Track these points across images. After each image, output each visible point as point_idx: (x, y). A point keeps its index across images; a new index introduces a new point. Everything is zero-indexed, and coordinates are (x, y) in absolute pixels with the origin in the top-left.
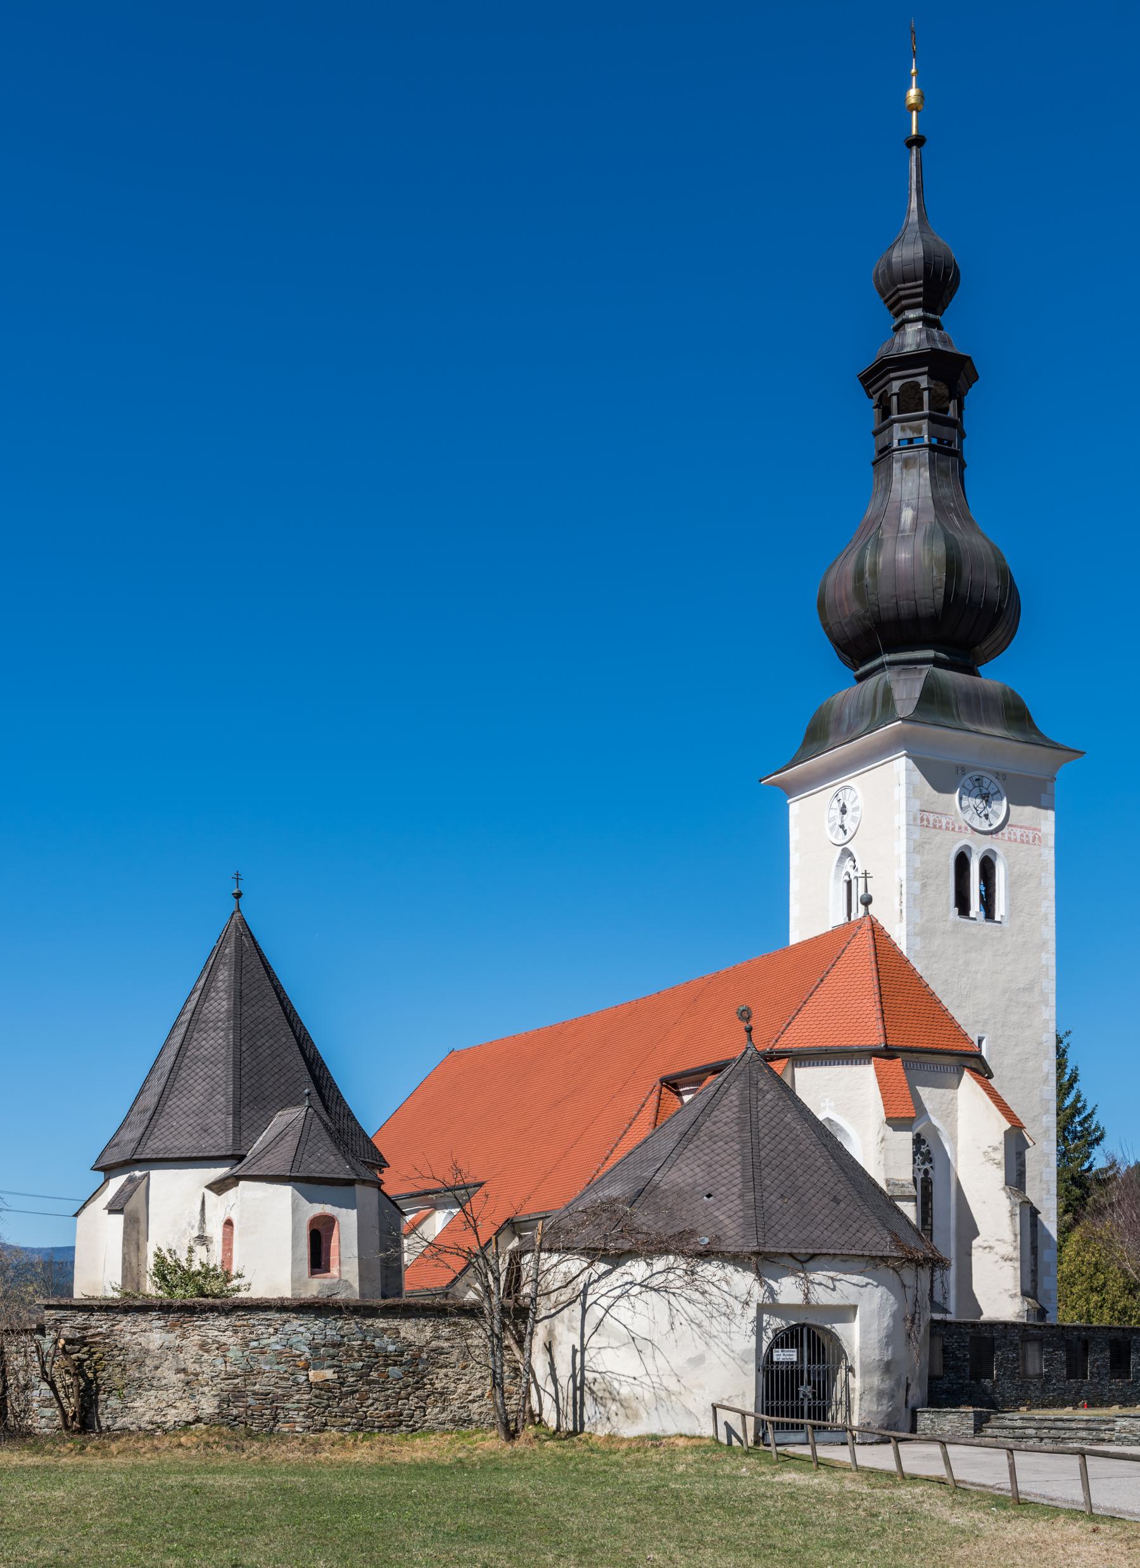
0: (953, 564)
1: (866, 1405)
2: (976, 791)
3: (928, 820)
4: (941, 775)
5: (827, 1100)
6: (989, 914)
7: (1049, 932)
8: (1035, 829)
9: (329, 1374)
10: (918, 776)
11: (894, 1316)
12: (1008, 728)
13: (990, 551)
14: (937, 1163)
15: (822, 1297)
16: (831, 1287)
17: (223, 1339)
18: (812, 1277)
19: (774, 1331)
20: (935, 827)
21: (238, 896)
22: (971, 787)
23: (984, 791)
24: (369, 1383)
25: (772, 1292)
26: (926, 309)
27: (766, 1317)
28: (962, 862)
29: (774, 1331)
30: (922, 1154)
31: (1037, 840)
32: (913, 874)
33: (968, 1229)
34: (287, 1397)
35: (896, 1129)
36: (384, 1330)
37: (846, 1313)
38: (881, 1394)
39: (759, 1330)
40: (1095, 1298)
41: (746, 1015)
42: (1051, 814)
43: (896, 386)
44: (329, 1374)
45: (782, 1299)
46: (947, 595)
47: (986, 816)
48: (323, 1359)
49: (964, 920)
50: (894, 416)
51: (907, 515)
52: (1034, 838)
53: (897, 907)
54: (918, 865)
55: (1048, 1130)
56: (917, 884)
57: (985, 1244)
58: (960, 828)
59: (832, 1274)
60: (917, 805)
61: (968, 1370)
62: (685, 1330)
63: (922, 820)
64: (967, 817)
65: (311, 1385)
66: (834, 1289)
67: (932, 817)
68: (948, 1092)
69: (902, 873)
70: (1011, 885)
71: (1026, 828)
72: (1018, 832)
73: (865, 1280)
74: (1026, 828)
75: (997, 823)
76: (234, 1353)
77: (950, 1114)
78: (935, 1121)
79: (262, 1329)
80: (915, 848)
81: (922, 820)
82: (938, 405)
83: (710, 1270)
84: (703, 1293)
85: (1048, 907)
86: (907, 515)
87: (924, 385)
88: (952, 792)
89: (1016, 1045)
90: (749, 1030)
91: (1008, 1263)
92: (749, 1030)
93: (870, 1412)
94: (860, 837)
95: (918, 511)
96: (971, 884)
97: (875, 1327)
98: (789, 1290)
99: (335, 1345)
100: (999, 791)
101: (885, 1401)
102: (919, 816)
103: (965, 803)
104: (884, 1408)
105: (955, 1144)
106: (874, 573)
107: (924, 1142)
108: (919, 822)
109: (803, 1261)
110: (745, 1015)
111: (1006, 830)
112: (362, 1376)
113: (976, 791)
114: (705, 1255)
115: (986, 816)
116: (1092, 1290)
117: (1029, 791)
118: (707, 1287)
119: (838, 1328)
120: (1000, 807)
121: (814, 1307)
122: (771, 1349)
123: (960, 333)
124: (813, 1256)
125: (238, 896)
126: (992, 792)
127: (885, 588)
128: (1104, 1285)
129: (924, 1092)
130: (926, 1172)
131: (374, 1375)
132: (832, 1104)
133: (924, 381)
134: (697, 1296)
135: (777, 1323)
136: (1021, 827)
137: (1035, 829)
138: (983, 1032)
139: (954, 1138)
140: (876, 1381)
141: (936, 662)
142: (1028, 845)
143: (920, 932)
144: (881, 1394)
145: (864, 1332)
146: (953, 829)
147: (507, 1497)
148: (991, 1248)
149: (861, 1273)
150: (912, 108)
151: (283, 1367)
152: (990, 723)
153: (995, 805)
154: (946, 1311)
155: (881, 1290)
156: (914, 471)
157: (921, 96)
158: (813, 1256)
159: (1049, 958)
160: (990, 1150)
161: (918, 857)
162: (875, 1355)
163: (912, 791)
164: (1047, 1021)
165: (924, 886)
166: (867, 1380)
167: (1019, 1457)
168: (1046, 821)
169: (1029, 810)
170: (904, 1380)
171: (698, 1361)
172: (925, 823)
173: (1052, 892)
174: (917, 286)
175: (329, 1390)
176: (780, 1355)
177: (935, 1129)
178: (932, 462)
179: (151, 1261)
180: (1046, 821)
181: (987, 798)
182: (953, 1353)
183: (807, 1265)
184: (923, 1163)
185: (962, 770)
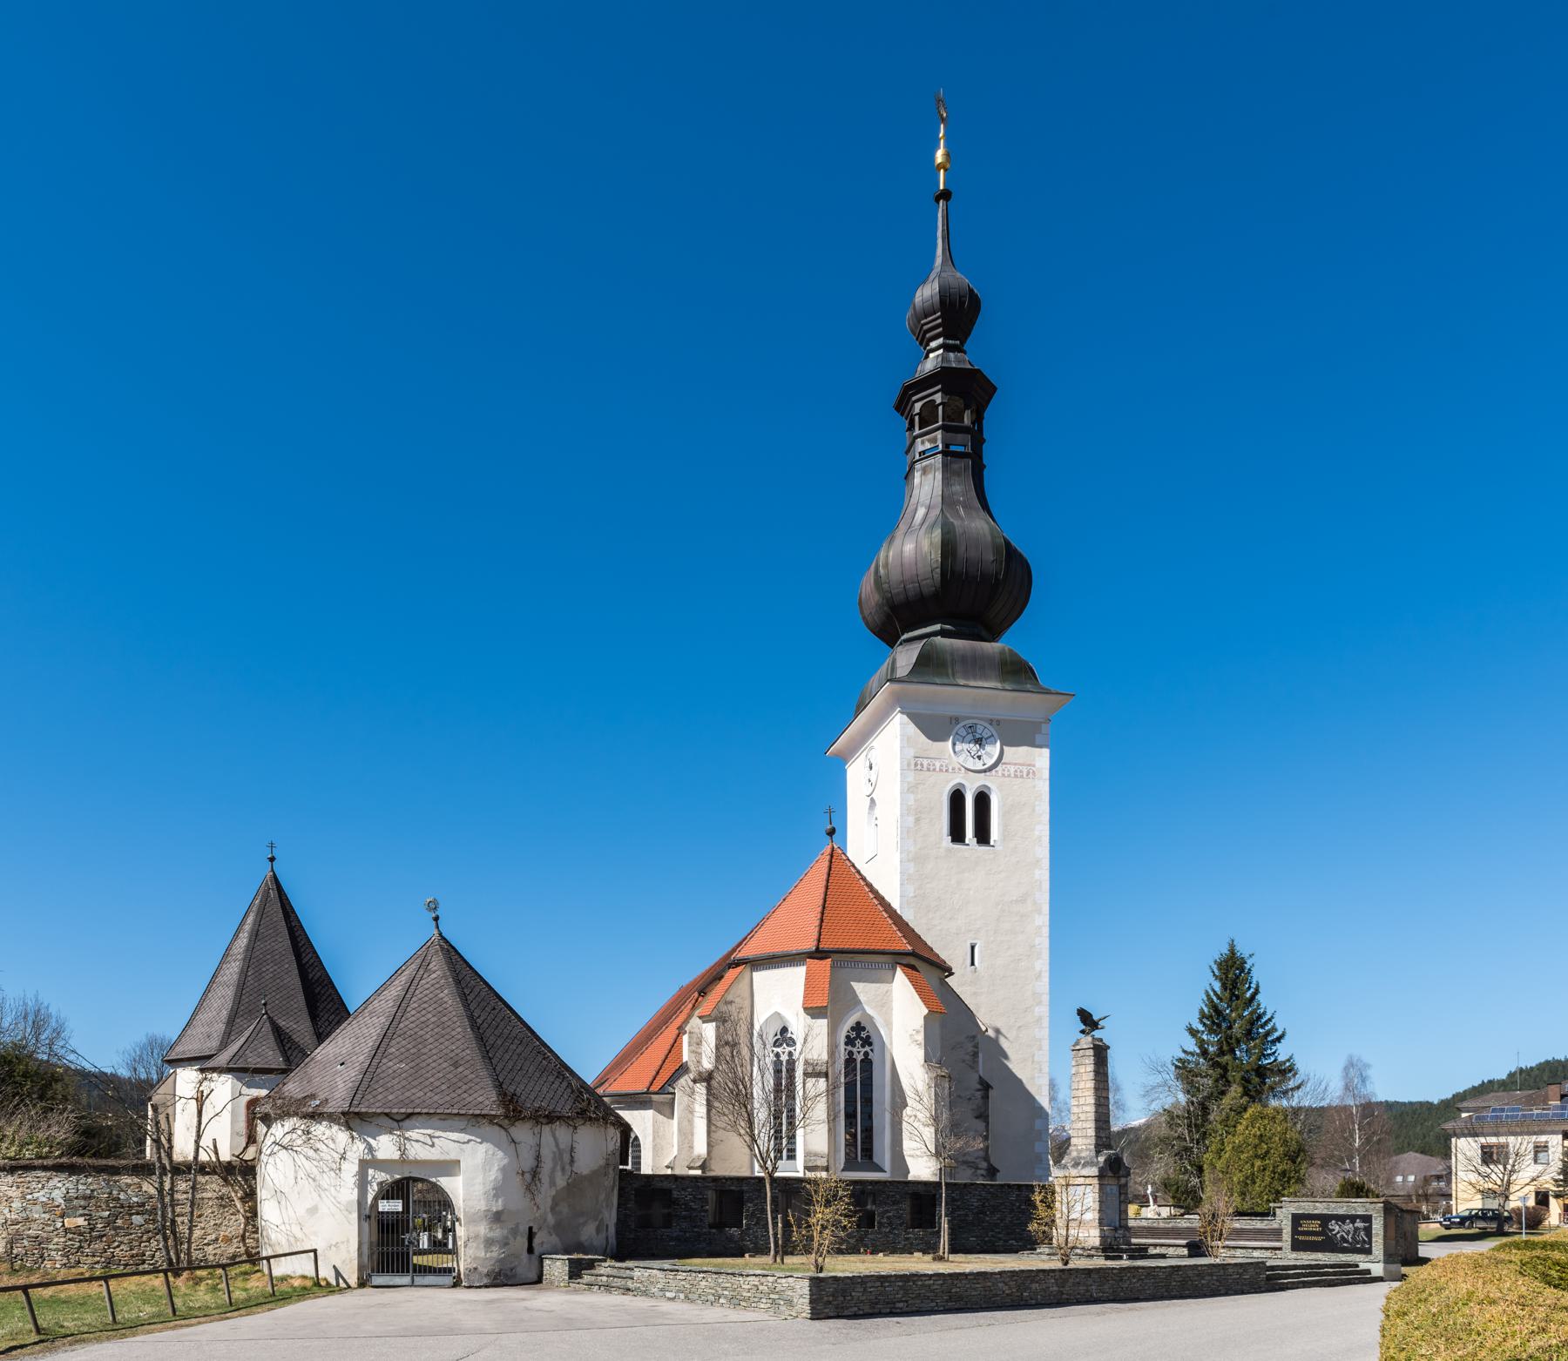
0: (948, 547)
1: (471, 1252)
2: (970, 737)
4: (934, 727)
6: (983, 836)
7: (1043, 851)
9: (81, 1221)
10: (912, 729)
11: (503, 1170)
12: (1003, 681)
14: (876, 1047)
15: (418, 1152)
16: (426, 1145)
17: (10, 1194)
18: (408, 1134)
19: (380, 1184)
21: (272, 859)
24: (115, 1229)
25: (370, 1149)
26: (946, 338)
27: (371, 1172)
28: (957, 798)
29: (380, 1184)
31: (1031, 774)
32: (906, 810)
33: (899, 1101)
34: (49, 1240)
35: (814, 1016)
36: (129, 1186)
37: (450, 1167)
38: (489, 1243)
39: (363, 1183)
40: (1258, 1163)
42: (1046, 752)
43: (918, 406)
44: (81, 1221)
45: (380, 1155)
46: (943, 574)
48: (75, 1208)
49: (984, 848)
50: (917, 432)
51: (921, 512)
54: (911, 802)
56: (911, 819)
59: (429, 1131)
60: (911, 752)
62: (305, 1184)
63: (916, 765)
64: (961, 759)
65: (67, 1231)
66: (433, 1146)
67: (925, 762)
68: (883, 987)
70: (1004, 815)
72: (1012, 769)
73: (468, 1137)
75: (990, 762)
76: (16, 1205)
77: (885, 1004)
78: (869, 1011)
79: (34, 1185)
80: (909, 789)
82: (952, 416)
83: (321, 1129)
84: (316, 1150)
85: (1042, 830)
86: (921, 512)
87: (939, 401)
88: (943, 739)
90: (436, 919)
92: (436, 919)
93: (475, 1258)
94: (887, 784)
95: (929, 508)
96: (969, 818)
97: (480, 1179)
98: (386, 1146)
99: (85, 1198)
101: (495, 1248)
103: (958, 747)
104: (495, 1254)
105: (891, 1030)
106: (886, 565)
107: (864, 1029)
109: (398, 1120)
110: (433, 906)
111: (999, 768)
112: (109, 1223)
113: (970, 737)
114: (315, 1116)
116: (1257, 1156)
117: (1018, 734)
118: (319, 1145)
119: (444, 1182)
120: (993, 750)
121: (411, 1162)
122: (375, 1199)
123: (978, 354)
124: (409, 1116)
125: (272, 859)
127: (895, 576)
128: (1267, 1152)
129: (860, 988)
131: (119, 1222)
133: (938, 398)
134: (311, 1153)
135: (382, 1176)
139: (889, 1024)
140: (483, 1229)
141: (943, 633)
142: (1022, 782)
143: (914, 861)
144: (489, 1243)
145: (467, 1185)
149: (462, 1131)
150: (940, 166)
151: (47, 1216)
152: (984, 677)
153: (988, 748)
154: (882, 1170)
155: (485, 1146)
156: (931, 476)
157: (947, 155)
158: (409, 1116)
159: (1043, 874)
161: (912, 797)
162: (481, 1205)
163: (906, 741)
164: (1040, 927)
165: (917, 820)
166: (472, 1229)
168: (1041, 758)
169: (1024, 750)
170: (524, 1229)
171: (313, 1211)
173: (1046, 817)
174: (936, 319)
175: (81, 1234)
176: (384, 1206)
177: (871, 1018)
178: (945, 466)
180: (1041, 758)
181: (979, 741)
183: (407, 1123)
185: (957, 720)
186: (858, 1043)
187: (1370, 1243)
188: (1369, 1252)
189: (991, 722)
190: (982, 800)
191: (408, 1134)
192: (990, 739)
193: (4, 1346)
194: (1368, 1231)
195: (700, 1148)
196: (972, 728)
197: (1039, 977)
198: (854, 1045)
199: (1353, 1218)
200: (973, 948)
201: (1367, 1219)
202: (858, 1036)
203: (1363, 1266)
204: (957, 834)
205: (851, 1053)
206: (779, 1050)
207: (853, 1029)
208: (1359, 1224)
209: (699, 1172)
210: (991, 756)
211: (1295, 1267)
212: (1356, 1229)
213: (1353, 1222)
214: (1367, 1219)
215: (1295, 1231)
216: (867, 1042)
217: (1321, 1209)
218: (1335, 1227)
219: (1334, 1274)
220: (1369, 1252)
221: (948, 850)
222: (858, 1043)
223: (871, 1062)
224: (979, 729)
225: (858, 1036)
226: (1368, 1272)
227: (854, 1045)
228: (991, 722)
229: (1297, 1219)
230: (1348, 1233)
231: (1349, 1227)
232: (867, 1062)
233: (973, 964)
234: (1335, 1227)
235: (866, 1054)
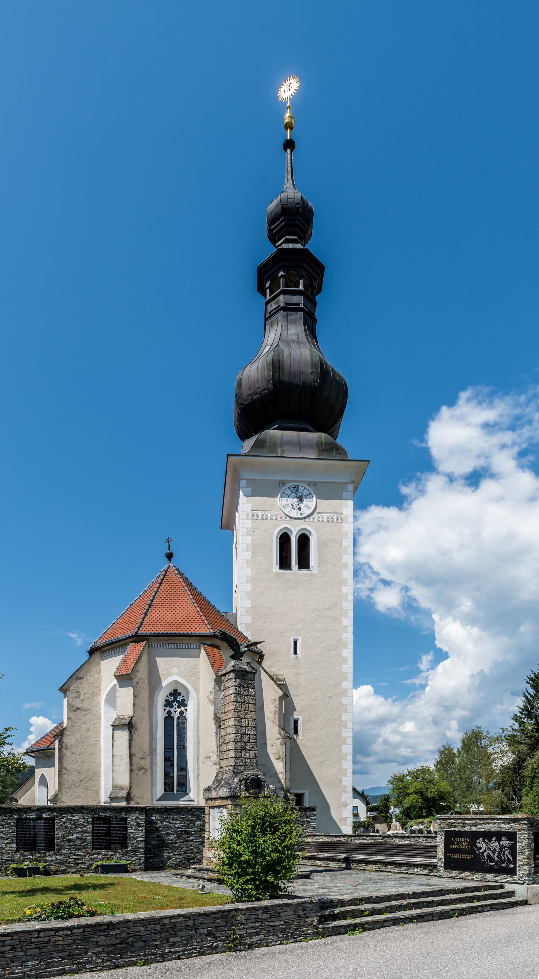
2: (294, 495)
3: (257, 516)
6: (304, 563)
8: (338, 513)
13: (289, 365)
20: (262, 519)
22: (289, 493)
23: (299, 494)
28: (284, 539)
31: (340, 519)
47: (300, 509)
49: (304, 572)
52: (337, 519)
58: (281, 518)
67: (260, 514)
71: (331, 513)
74: (331, 513)
75: (307, 512)
81: (253, 516)
88: (276, 496)
89: (322, 642)
100: (310, 493)
102: (251, 514)
108: (250, 517)
111: (315, 515)
115: (300, 509)
120: (309, 504)
136: (328, 513)
137: (338, 513)
138: (297, 635)
147: (223, 880)
148: (210, 757)
172: (255, 517)
179: (348, 734)
184: (179, 707)
185: (283, 483)
186: (175, 704)
187: (515, 863)
188: (512, 872)
189: (309, 484)
190: (304, 540)
192: (309, 495)
193: (4, 890)
194: (513, 849)
196: (295, 489)
197: (345, 660)
198: (172, 707)
199: (499, 835)
200: (296, 643)
201: (512, 836)
203: (508, 887)
204: (284, 563)
205: (169, 713)
208: (505, 842)
209: (124, 804)
210: (309, 508)
211: (369, 900)
212: (502, 848)
213: (499, 840)
214: (512, 836)
215: (447, 850)
217: (469, 826)
218: (482, 844)
219: (461, 900)
220: (512, 872)
221: (278, 574)
222: (175, 704)
224: (301, 489)
225: (175, 700)
226: (511, 894)
227: (172, 707)
228: (309, 484)
229: (450, 836)
230: (494, 851)
231: (495, 845)
233: (295, 653)
234: (482, 844)
235: (182, 713)
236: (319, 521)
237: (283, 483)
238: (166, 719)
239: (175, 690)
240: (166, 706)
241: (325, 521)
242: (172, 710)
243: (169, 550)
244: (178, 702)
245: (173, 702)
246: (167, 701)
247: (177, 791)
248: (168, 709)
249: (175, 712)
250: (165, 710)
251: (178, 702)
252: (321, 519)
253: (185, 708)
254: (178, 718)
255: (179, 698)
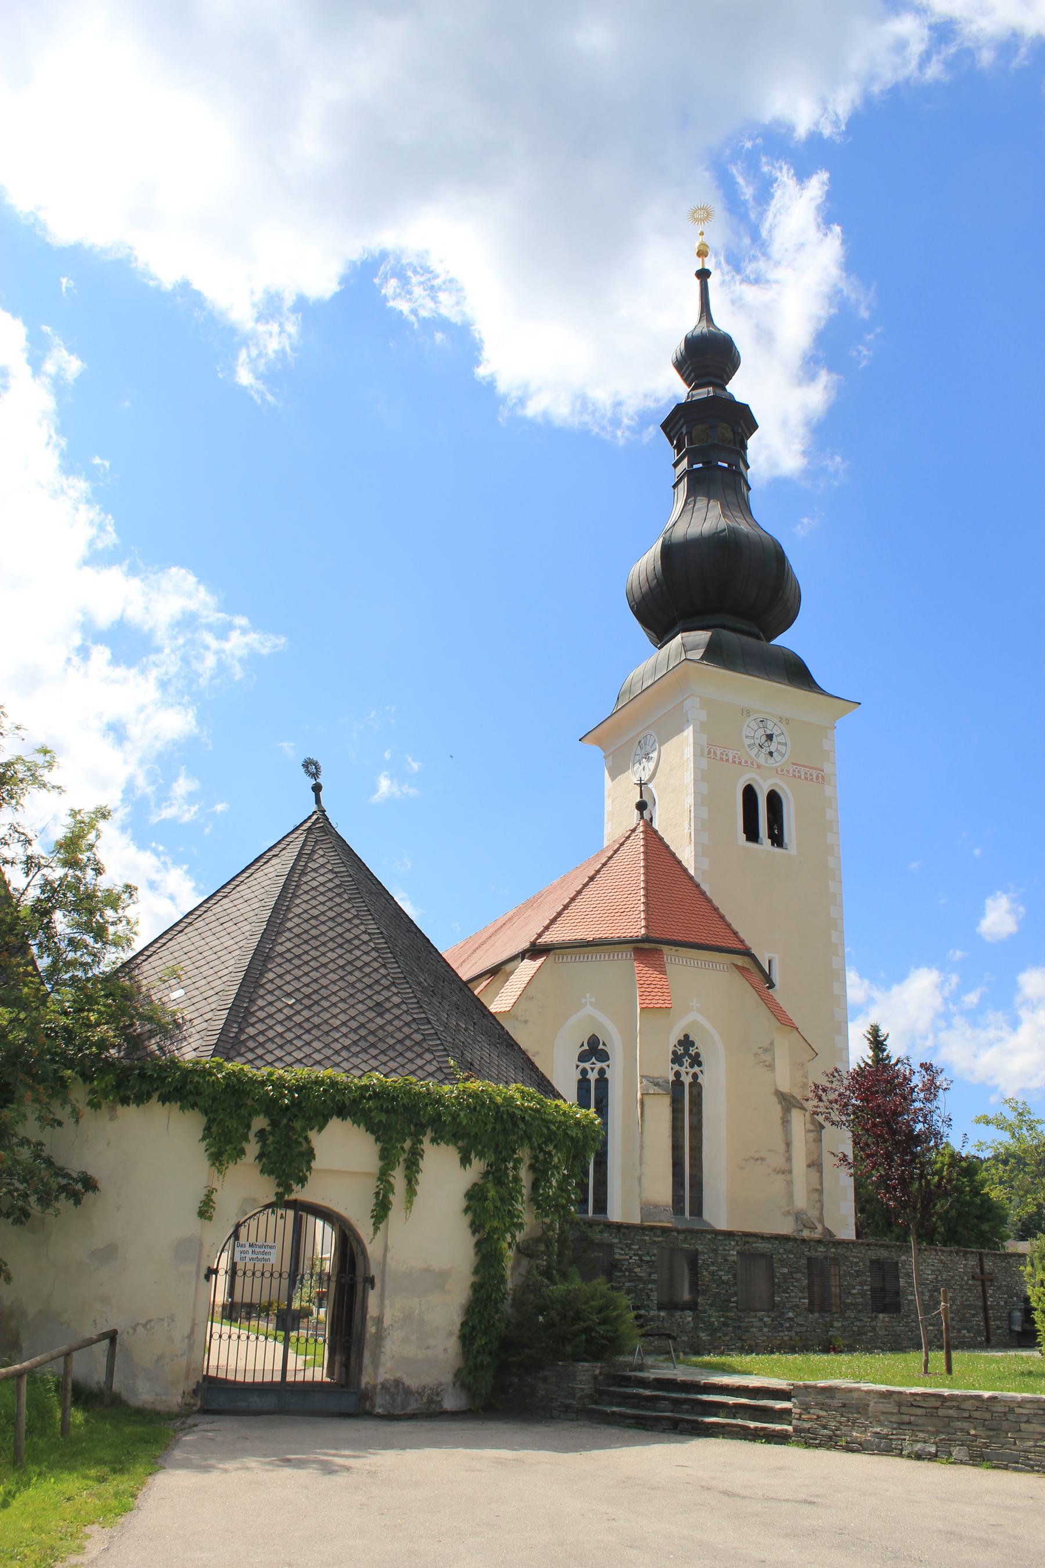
3: (715, 753)
5: (588, 995)
6: (777, 840)
23: (769, 732)
28: (749, 794)
30: (690, 1056)
41: (313, 769)
49: (777, 850)
53: (686, 831)
55: (609, 796)
57: (757, 1156)
58: (746, 762)
61: (654, 1296)
67: (803, 770)
69: (690, 800)
81: (709, 752)
90: (317, 789)
91: (781, 1176)
92: (317, 789)
107: (692, 1044)
126: (776, 733)
130: (695, 1076)
132: (593, 1000)
146: (740, 763)
148: (763, 1159)
160: (761, 1051)
167: (954, 1355)
182: (630, 1271)
184: (692, 1066)
186: (687, 1061)
191: (1005, 1137)
195: (801, 1200)
202: (686, 1052)
204: (751, 833)
206: (587, 1065)
207: (680, 1043)
216: (696, 1061)
222: (687, 1061)
223: (700, 1086)
224: (770, 725)
225: (686, 1052)
227: (681, 1065)
228: (781, 719)
232: (696, 1087)
235: (602, 1072)
236: (794, 776)
237: (748, 713)
238: (580, 1082)
239: (686, 1036)
240: (673, 1061)
241: (731, 760)
242: (683, 1070)
243: (641, 797)
244: (683, 1056)
245: (683, 1056)
246: (674, 1053)
247: (594, 1212)
248: (676, 1067)
249: (592, 1069)
250: (578, 1066)
251: (690, 1056)
252: (796, 774)
253: (607, 1063)
254: (597, 1080)
255: (681, 1050)
